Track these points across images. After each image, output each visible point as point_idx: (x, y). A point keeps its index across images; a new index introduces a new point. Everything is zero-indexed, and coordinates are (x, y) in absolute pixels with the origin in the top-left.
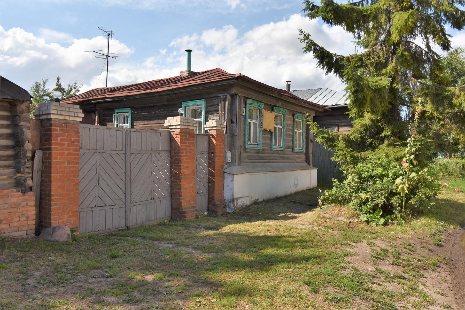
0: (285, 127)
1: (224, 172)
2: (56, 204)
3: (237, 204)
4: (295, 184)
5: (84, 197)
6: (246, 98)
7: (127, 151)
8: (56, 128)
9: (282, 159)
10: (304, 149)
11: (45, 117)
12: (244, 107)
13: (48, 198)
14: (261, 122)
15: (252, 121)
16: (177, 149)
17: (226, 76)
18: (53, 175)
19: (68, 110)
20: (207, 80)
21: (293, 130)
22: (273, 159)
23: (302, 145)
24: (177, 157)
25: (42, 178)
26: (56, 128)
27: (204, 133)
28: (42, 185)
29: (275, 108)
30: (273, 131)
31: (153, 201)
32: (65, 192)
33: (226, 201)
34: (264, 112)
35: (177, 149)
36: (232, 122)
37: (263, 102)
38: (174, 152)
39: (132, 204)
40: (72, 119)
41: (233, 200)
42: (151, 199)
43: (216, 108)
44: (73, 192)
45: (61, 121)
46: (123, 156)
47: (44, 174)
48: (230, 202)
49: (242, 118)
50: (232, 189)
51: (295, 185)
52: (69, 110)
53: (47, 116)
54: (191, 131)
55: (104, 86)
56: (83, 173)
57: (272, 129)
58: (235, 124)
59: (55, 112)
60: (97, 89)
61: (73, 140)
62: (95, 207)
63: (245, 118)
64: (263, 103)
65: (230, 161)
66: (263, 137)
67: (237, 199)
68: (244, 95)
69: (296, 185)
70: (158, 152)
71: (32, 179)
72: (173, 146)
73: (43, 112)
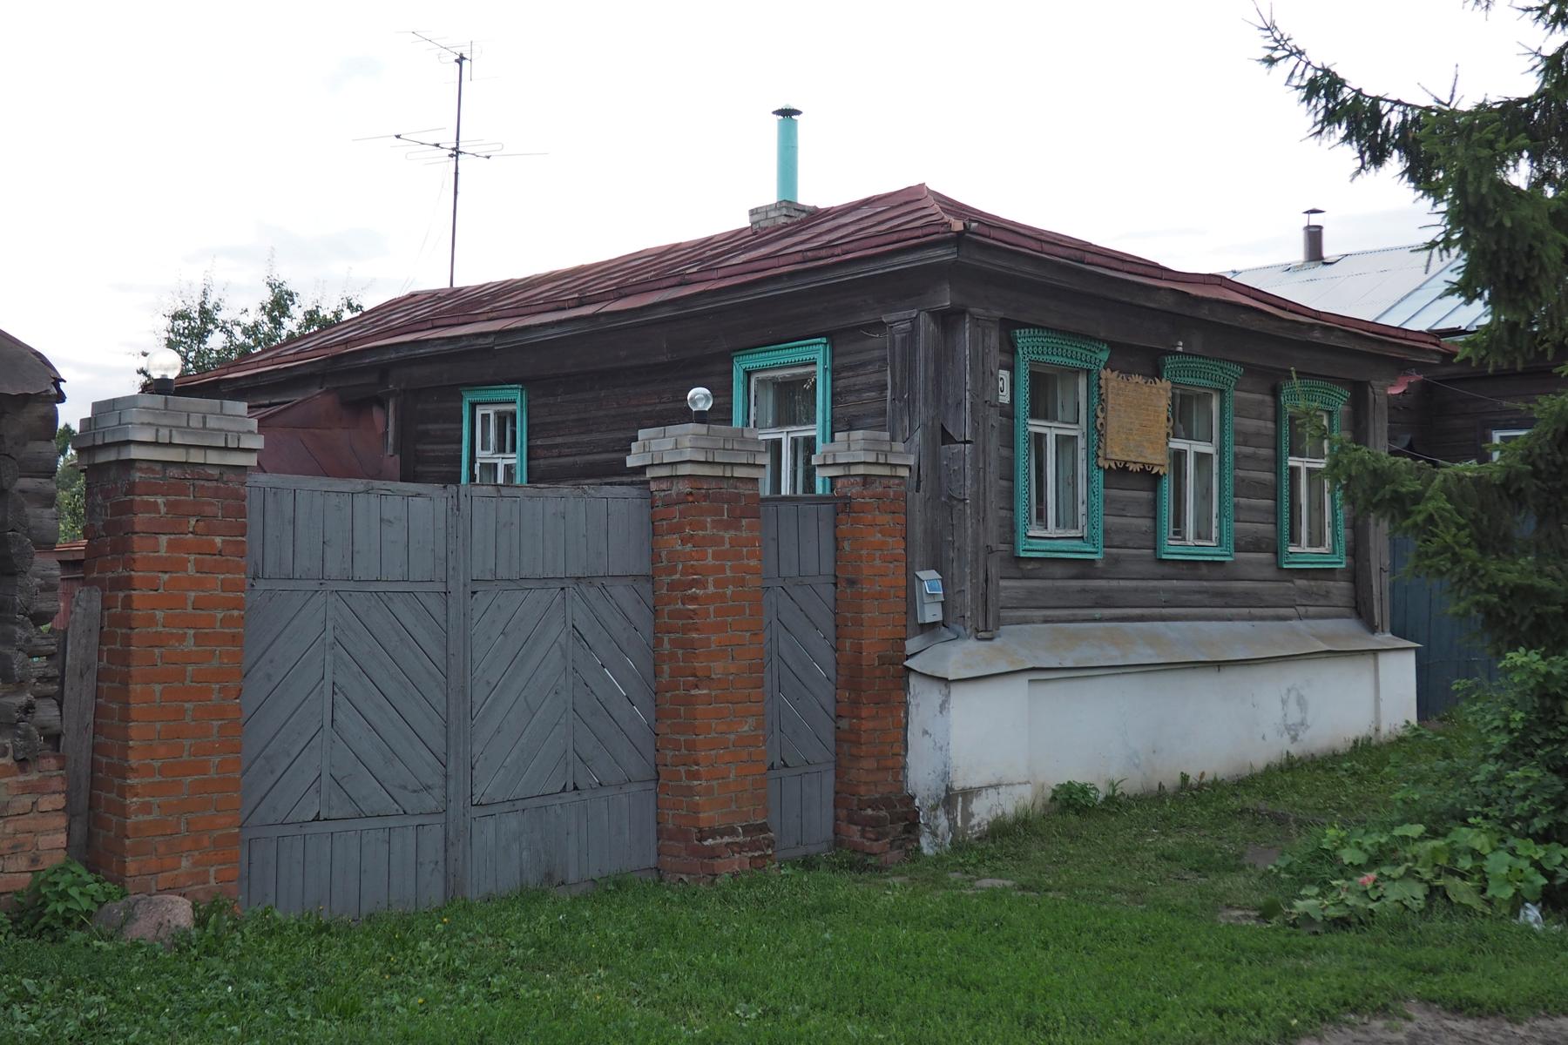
0: (1231, 449)
1: (909, 670)
2: (146, 808)
3: (968, 816)
4: (1290, 722)
5: (273, 778)
6: (1008, 327)
7: (451, 583)
8: (152, 499)
9: (1218, 601)
10: (1342, 548)
11: (111, 456)
12: (1002, 367)
13: (117, 781)
14: (1097, 432)
15: (1051, 432)
16: (680, 567)
17: (908, 234)
18: (136, 688)
19: (185, 425)
20: (830, 252)
21: (1277, 461)
22: (1167, 605)
23: (1328, 532)
24: (680, 606)
25: (99, 700)
26: (152, 499)
27: (828, 492)
28: (98, 729)
29: (1169, 361)
30: (1165, 470)
31: (570, 796)
32: (185, 757)
33: (917, 802)
34: (1112, 384)
35: (680, 567)
36: (947, 438)
37: (1102, 335)
38: (667, 579)
39: (477, 812)
40: (214, 458)
41: (952, 798)
42: (564, 790)
43: (873, 378)
44: (216, 760)
45: (173, 472)
46: (434, 604)
47: (105, 685)
48: (934, 808)
49: (995, 419)
50: (942, 748)
51: (1288, 728)
52: (205, 423)
53: (119, 453)
54: (745, 490)
55: (439, 282)
56: (269, 677)
57: (1157, 458)
58: (956, 448)
59: (148, 436)
60: (413, 295)
61: (219, 545)
62: (317, 819)
63: (1009, 412)
64: (1103, 341)
65: (939, 618)
66: (1107, 501)
67: (968, 794)
68: (1000, 314)
69: (1294, 733)
70: (597, 582)
71: (60, 705)
72: (664, 554)
73: (94, 440)
